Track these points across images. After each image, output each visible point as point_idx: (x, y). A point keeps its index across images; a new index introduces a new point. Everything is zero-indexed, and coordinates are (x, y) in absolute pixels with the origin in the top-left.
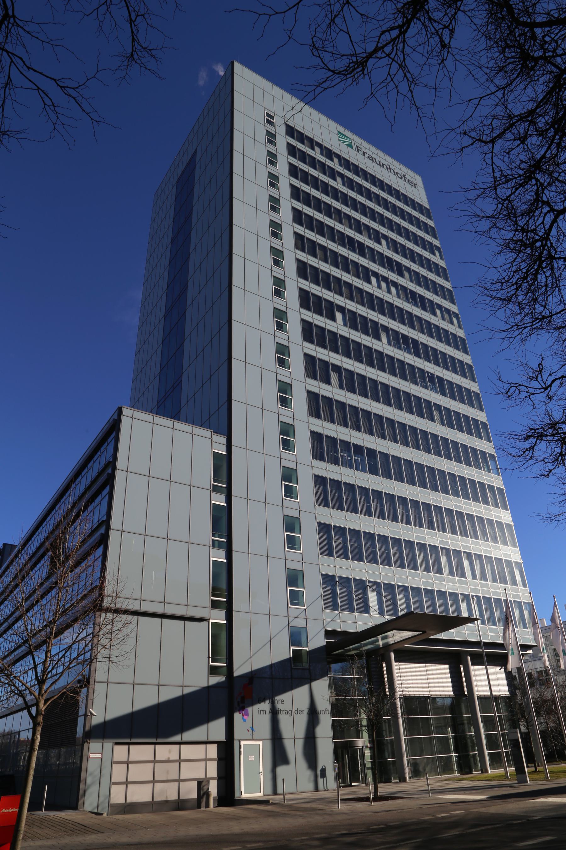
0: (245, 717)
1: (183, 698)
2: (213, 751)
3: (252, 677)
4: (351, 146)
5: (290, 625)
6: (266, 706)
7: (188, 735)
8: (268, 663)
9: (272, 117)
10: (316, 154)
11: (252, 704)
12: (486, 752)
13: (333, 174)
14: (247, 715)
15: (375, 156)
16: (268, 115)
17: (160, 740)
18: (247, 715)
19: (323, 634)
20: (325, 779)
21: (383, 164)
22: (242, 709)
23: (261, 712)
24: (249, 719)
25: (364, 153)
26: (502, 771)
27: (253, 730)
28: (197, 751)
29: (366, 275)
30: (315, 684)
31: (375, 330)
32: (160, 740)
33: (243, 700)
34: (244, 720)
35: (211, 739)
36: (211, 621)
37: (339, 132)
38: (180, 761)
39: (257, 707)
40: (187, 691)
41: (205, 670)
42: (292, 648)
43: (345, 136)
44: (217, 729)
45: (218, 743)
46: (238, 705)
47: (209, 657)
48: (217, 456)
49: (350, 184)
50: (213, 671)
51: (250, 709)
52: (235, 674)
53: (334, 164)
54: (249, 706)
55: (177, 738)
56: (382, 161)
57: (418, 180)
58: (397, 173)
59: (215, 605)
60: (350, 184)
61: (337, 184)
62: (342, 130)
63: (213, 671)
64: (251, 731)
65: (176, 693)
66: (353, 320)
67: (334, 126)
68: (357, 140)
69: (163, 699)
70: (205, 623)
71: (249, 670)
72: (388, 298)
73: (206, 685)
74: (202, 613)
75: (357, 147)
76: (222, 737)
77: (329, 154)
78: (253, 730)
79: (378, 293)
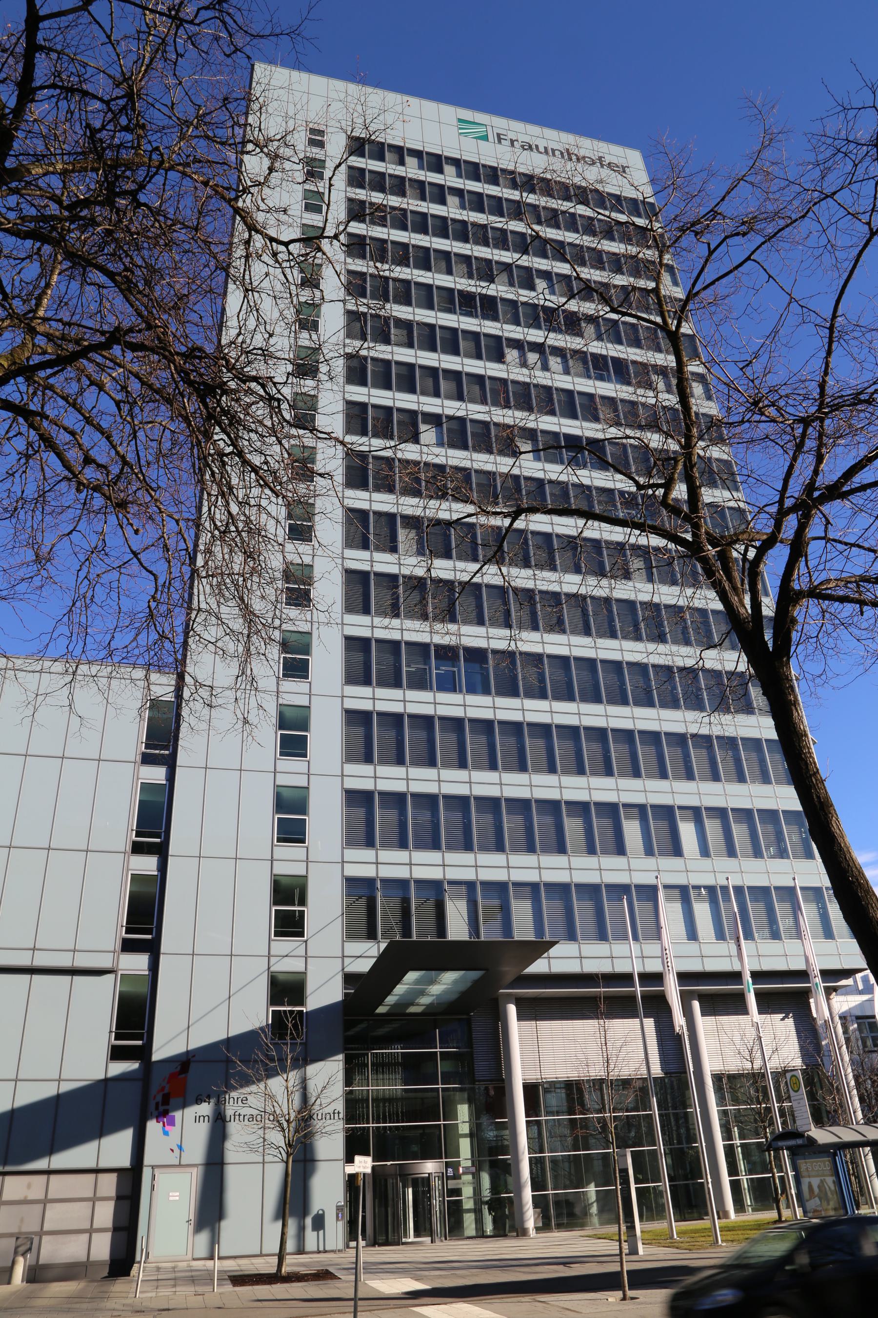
0: (167, 1128)
1: (58, 1100)
2: (109, 1184)
3: (185, 1063)
4: (485, 138)
5: (272, 969)
6: (205, 1109)
7: (60, 1160)
8: (223, 1036)
9: (321, 133)
10: (411, 170)
11: (184, 1106)
12: (633, 1187)
13: (440, 194)
14: (172, 1123)
15: (534, 142)
16: (313, 131)
17: (8, 1168)
18: (172, 1123)
19: (339, 980)
20: (321, 1232)
21: (553, 151)
22: (163, 1113)
23: (197, 1119)
24: (174, 1131)
25: (512, 142)
26: (772, 1215)
27: (180, 1148)
28: (83, 1185)
29: (495, 349)
30: (312, 1069)
31: (506, 442)
32: (8, 1168)
33: (166, 1100)
34: (166, 1133)
35: (103, 1165)
36: (120, 973)
37: (460, 120)
38: (45, 1202)
39: (192, 1111)
40: (65, 1087)
41: (103, 1051)
42: (271, 1009)
43: (474, 123)
44: (116, 1148)
45: (119, 1171)
46: (157, 1108)
47: (111, 1032)
48: (155, 704)
49: (477, 202)
50: (117, 1054)
51: (178, 1115)
52: (155, 1057)
53: (450, 178)
54: (176, 1109)
55: (41, 1164)
56: (552, 145)
57: (634, 158)
58: (584, 157)
59: (128, 946)
60: (477, 202)
61: (452, 210)
62: (467, 114)
63: (117, 1054)
64: (177, 1151)
65: (48, 1091)
66: (458, 433)
67: (450, 113)
68: (500, 123)
69: (20, 1102)
70: (111, 977)
71: (184, 1050)
72: (564, 382)
73: (102, 1077)
74: (105, 962)
75: (498, 135)
76: (125, 1161)
77: (436, 163)
78: (180, 1148)
79: (519, 375)
